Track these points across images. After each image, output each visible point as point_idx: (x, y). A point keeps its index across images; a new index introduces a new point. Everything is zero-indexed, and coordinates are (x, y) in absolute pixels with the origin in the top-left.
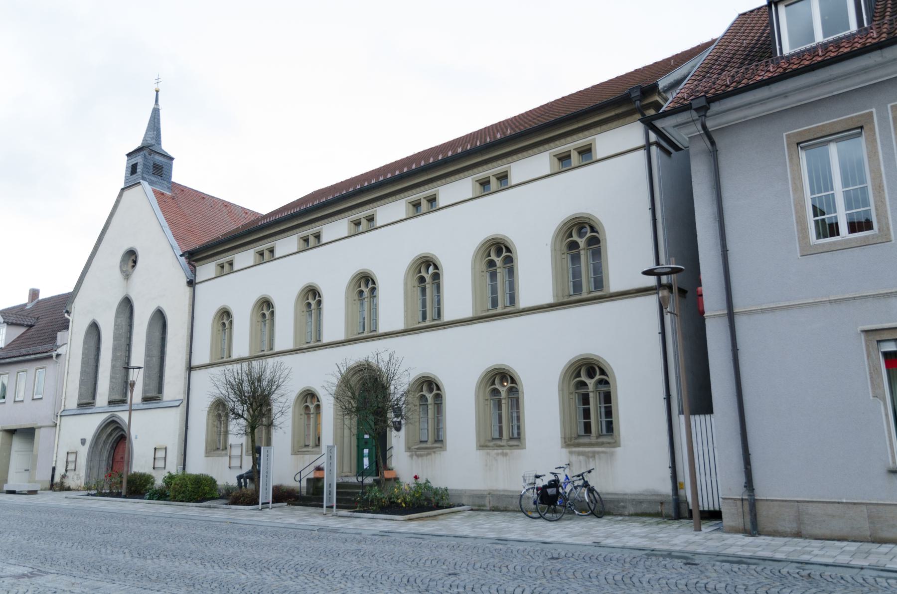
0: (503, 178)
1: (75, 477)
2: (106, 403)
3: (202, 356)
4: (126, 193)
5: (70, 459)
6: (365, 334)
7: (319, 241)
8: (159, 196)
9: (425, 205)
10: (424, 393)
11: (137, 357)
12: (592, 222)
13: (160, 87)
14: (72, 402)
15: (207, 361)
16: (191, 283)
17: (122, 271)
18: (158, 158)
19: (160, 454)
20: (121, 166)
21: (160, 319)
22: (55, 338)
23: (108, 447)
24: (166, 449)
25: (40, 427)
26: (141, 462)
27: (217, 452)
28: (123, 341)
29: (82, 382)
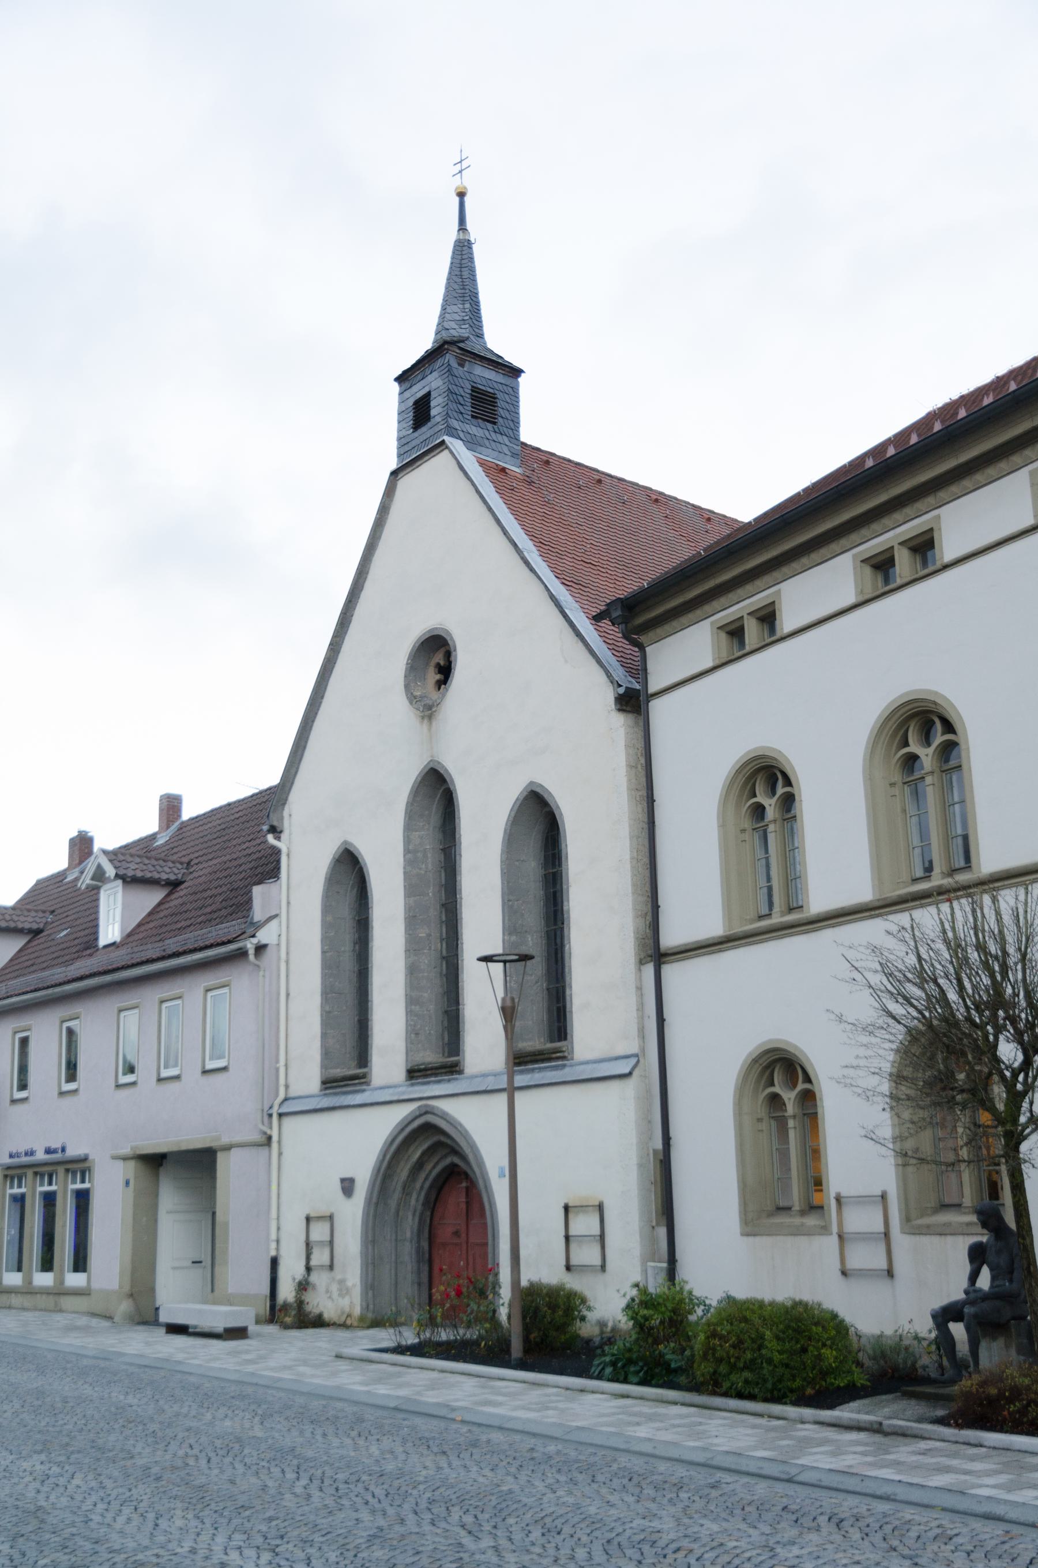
0: (923, 546)
1: (334, 1288)
2: (399, 1074)
3: (695, 908)
4: (405, 482)
5: (315, 1236)
6: (776, 919)
7: (772, 630)
8: (497, 473)
9: (904, 563)
10: (777, 1089)
11: (499, 927)
12: (940, 710)
13: (468, 181)
14: (306, 1075)
15: (715, 927)
16: (633, 702)
17: (412, 698)
18: (483, 374)
19: (584, 1225)
20: (387, 408)
21: (539, 822)
22: (247, 904)
23: (416, 1200)
24: (600, 1207)
25: (228, 1148)
26: (533, 1253)
27: (779, 1220)
28: (432, 895)
29: (328, 1020)
